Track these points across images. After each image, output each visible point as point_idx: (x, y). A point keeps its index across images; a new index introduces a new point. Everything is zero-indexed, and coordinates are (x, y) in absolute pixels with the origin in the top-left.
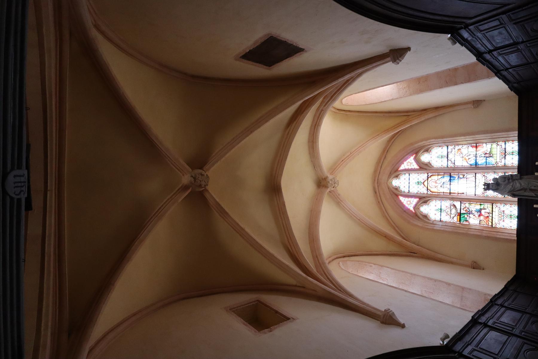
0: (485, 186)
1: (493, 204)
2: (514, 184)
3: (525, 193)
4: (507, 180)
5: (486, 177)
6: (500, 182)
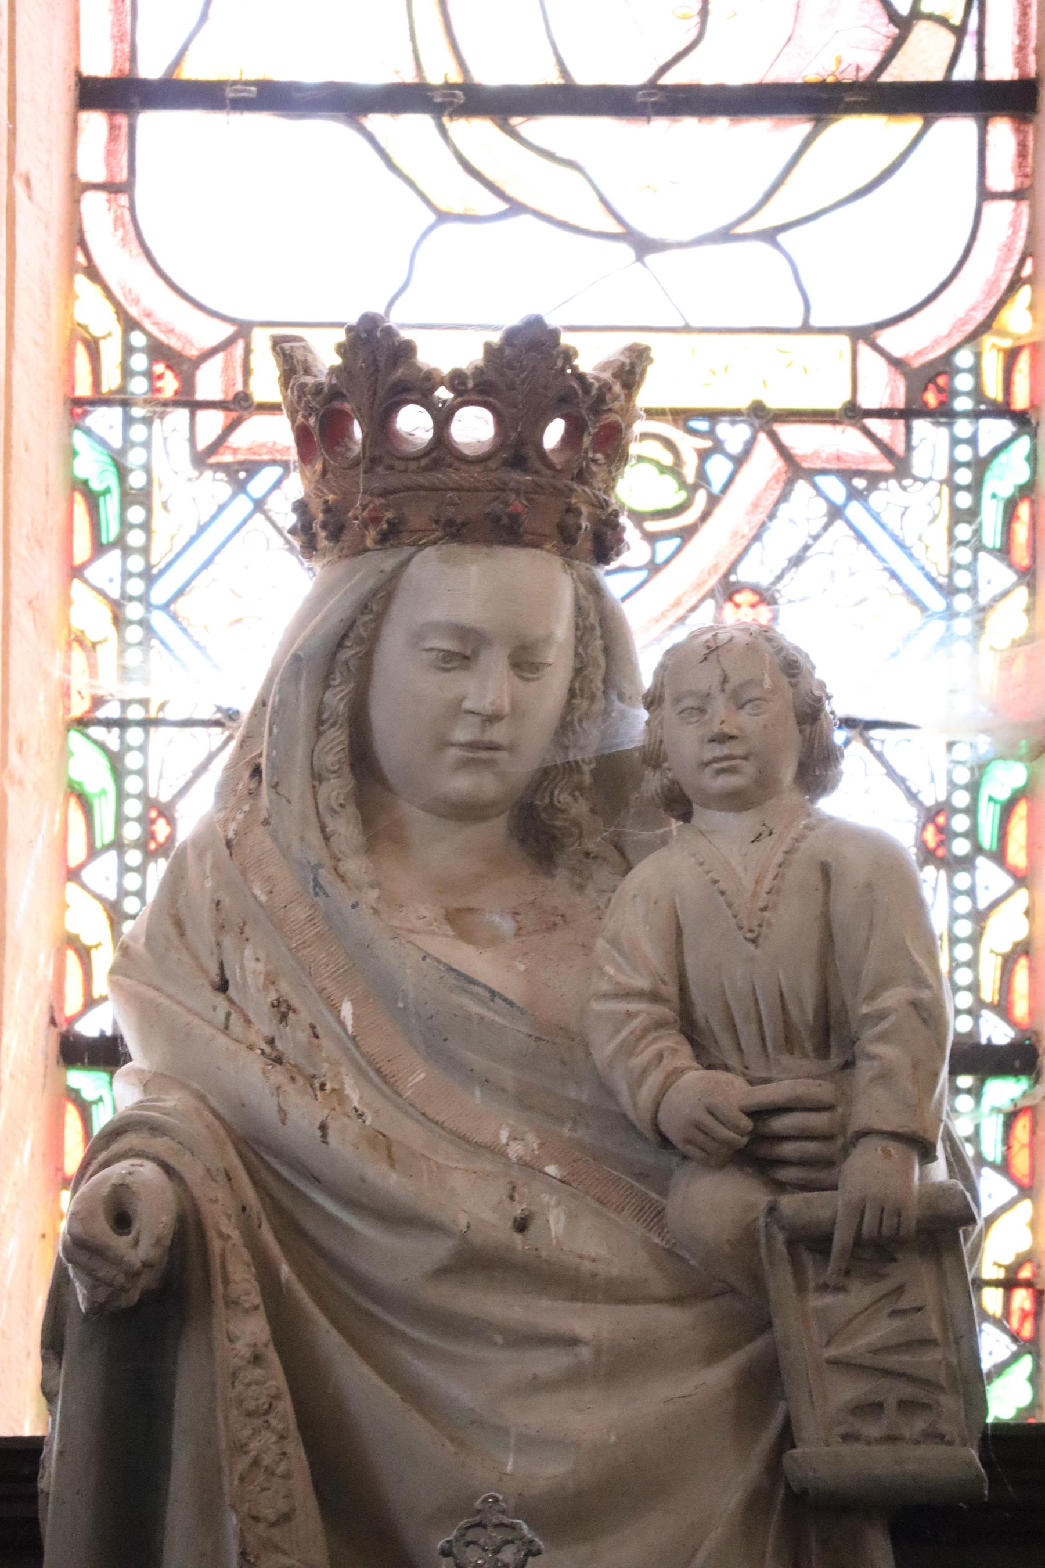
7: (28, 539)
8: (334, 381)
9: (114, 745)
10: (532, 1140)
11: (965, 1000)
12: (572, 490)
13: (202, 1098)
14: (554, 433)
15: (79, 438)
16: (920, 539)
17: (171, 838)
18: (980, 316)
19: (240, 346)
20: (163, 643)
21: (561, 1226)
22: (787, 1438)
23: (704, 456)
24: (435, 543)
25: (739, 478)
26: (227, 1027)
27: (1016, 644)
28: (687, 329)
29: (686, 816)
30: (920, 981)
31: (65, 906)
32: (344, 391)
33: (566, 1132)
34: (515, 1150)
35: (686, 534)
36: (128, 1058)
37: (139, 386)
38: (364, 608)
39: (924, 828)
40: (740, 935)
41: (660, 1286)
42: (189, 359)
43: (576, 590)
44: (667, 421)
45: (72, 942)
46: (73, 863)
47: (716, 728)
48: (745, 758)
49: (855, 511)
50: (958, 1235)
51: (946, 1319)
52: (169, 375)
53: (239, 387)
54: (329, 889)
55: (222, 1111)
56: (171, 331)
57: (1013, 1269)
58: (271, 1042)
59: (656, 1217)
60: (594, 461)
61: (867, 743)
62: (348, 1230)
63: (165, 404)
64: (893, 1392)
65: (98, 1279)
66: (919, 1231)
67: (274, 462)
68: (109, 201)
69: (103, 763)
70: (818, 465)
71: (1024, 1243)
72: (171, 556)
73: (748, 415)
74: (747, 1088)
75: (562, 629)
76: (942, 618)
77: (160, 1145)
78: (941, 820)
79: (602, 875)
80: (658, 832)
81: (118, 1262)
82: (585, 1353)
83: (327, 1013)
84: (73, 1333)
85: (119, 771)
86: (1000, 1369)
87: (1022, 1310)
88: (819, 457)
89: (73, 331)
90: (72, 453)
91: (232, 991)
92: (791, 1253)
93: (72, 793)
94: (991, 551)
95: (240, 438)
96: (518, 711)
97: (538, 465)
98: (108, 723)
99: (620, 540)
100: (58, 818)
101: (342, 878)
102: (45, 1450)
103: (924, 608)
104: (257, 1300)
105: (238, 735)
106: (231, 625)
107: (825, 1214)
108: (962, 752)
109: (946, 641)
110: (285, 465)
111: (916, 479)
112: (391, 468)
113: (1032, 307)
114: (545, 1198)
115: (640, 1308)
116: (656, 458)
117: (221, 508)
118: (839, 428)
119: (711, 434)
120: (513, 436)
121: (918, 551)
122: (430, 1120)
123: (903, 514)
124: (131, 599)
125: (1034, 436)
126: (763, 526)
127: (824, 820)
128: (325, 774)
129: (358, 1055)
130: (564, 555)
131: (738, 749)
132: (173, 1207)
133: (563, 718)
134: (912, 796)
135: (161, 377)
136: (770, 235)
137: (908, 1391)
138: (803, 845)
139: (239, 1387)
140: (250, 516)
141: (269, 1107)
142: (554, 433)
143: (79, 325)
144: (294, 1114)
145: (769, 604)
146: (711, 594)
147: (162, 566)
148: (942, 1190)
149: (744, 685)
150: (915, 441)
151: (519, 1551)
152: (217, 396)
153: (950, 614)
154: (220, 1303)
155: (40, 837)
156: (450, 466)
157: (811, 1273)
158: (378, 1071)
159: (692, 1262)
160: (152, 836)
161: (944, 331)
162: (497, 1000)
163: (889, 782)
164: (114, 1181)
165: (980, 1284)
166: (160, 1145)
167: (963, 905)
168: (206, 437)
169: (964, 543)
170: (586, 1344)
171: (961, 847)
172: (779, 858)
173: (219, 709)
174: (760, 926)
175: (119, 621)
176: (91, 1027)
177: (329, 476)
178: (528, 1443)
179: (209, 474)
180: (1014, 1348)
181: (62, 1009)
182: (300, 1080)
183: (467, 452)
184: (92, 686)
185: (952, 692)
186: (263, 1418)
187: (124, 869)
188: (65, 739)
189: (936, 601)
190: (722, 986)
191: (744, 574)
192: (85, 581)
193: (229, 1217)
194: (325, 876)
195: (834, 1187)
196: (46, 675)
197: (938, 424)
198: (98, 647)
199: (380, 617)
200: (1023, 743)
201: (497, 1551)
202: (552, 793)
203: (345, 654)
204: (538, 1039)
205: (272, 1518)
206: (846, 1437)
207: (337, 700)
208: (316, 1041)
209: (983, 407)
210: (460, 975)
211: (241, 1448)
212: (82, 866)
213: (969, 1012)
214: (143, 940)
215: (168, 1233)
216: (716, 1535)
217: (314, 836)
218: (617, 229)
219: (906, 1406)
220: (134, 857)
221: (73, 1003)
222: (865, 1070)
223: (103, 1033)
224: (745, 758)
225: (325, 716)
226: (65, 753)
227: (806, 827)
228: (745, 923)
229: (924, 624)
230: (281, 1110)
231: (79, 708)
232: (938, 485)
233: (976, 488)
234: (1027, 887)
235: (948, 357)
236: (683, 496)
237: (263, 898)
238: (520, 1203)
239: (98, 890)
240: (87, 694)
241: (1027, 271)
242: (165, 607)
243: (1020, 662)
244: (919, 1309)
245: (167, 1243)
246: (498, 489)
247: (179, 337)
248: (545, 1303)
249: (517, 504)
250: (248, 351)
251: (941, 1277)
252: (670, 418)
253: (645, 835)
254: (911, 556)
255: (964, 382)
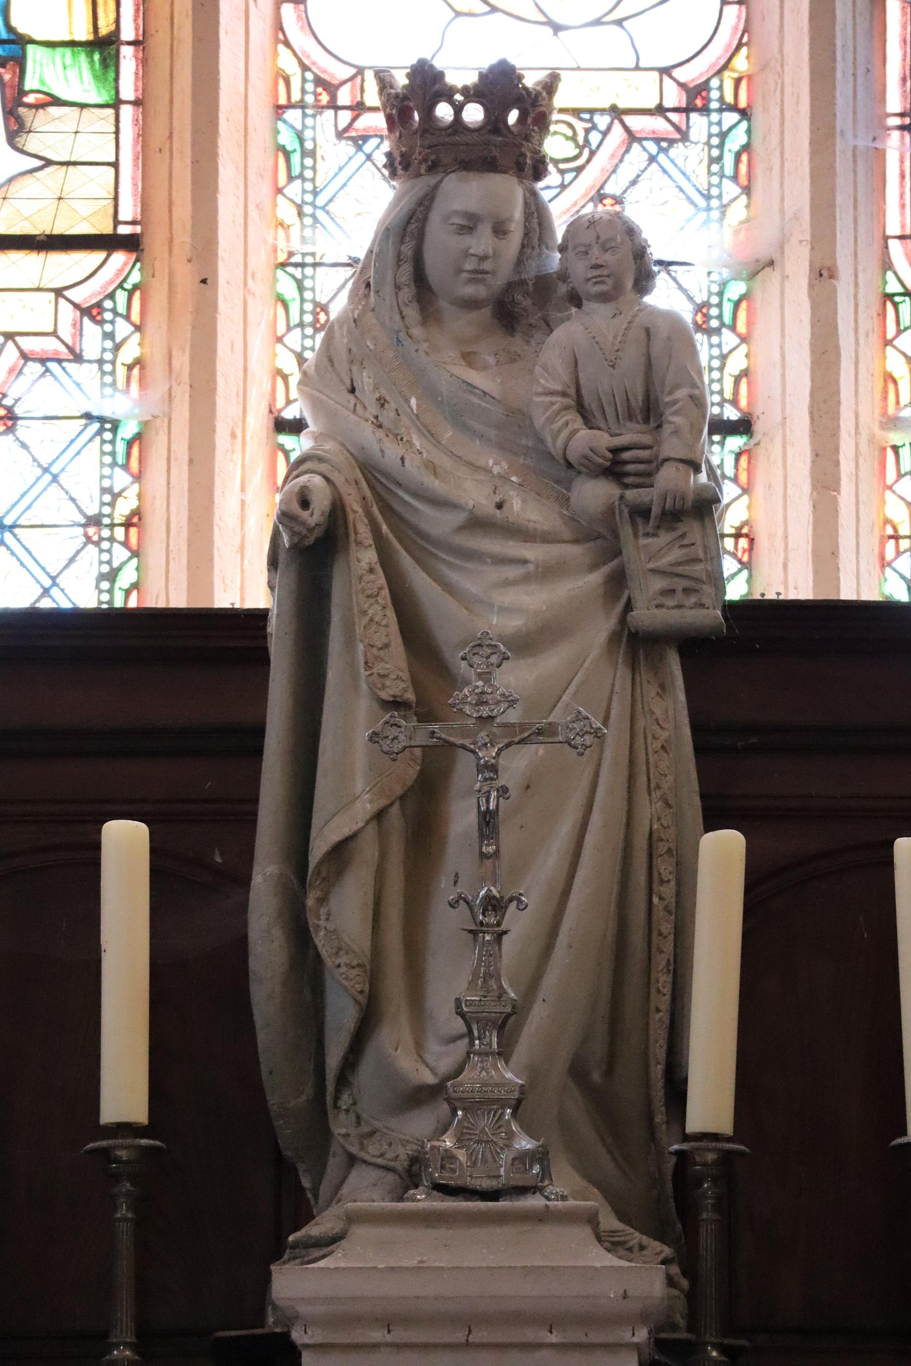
0: (473, 94)
1: (131, 244)
2: (532, 552)
3: (364, 706)
4: (603, 440)
5: (658, 124)
6: (559, 333)
7: (256, 174)
8: (405, 92)
9: (299, 276)
10: (505, 465)
11: (716, 398)
12: (522, 145)
13: (343, 445)
14: (513, 117)
15: (280, 125)
16: (694, 172)
17: (327, 321)
18: (722, 62)
19: (359, 79)
20: (322, 225)
21: (519, 506)
22: (629, 607)
23: (587, 131)
24: (454, 171)
25: (605, 142)
26: (355, 410)
27: (741, 223)
28: (578, 69)
29: (579, 306)
30: (694, 386)
31: (275, 355)
32: (410, 96)
33: (521, 461)
34: (496, 470)
35: (579, 170)
36: (307, 426)
37: (309, 99)
38: (420, 203)
39: (696, 314)
40: (606, 363)
41: (567, 534)
42: (334, 85)
43: (524, 194)
44: (570, 114)
45: (279, 373)
46: (279, 334)
47: (594, 262)
48: (608, 276)
49: (662, 158)
50: (712, 508)
51: (706, 549)
52: (324, 93)
53: (359, 99)
54: (405, 343)
55: (353, 451)
56: (325, 72)
57: (740, 528)
58: (376, 417)
59: (565, 501)
60: (533, 130)
61: (668, 273)
62: (416, 510)
63: (323, 107)
64: (681, 583)
65: (294, 532)
66: (693, 507)
67: (376, 136)
68: (295, 8)
69: (294, 285)
70: (644, 135)
71: (744, 516)
72: (326, 182)
73: (609, 111)
74: (610, 438)
75: (518, 214)
76: (704, 210)
77: (323, 467)
78: (704, 310)
79: (538, 336)
80: (565, 314)
81: (303, 523)
82: (531, 567)
83: (403, 403)
84: (282, 557)
85: (301, 288)
86: (733, 576)
87: (743, 548)
88: (644, 132)
89: (277, 72)
90: (277, 132)
91: (357, 393)
92: (630, 517)
93: (279, 300)
94: (728, 178)
95: (359, 124)
96: (496, 254)
97: (505, 132)
98: (296, 265)
99: (546, 170)
100: (272, 312)
101: (411, 337)
102: (270, 614)
103: (696, 206)
104: (371, 542)
105: (358, 271)
106: (355, 216)
107: (647, 499)
108: (715, 277)
109: (707, 221)
110: (381, 137)
111: (692, 142)
112: (433, 134)
113: (748, 57)
114: (511, 493)
115: (558, 545)
116: (564, 132)
117: (350, 159)
118: (654, 117)
119: (591, 120)
120: (493, 118)
121: (693, 178)
122: (455, 455)
123: (686, 159)
124: (307, 203)
125: (749, 120)
126: (617, 166)
127: (647, 307)
128: (402, 286)
129: (419, 425)
130: (518, 177)
131: (605, 272)
132: (330, 497)
133: (518, 259)
134: (690, 299)
135: (320, 94)
136: (619, 23)
137: (686, 583)
138: (637, 319)
139: (363, 584)
140: (364, 163)
141: (376, 447)
142: (513, 117)
143: (280, 69)
144: (388, 452)
145: (620, 204)
146: (592, 199)
147: (322, 187)
148: (705, 487)
149: (607, 240)
150: (691, 124)
151: (499, 657)
152: (348, 103)
153: (709, 209)
154: (353, 545)
155: (263, 321)
156: (462, 133)
157: (640, 528)
158: (429, 431)
159: (583, 523)
160: (318, 321)
161: (705, 69)
162: (487, 396)
163: (679, 292)
164: (300, 484)
165: (723, 536)
166: (323, 467)
167: (716, 352)
168: (342, 125)
169: (715, 174)
170: (531, 562)
171: (714, 323)
172: (625, 325)
173: (350, 258)
174: (616, 359)
175: (301, 214)
176: (290, 413)
177: (403, 138)
178: (504, 610)
179: (344, 142)
180: (739, 566)
181: (275, 405)
182: (391, 436)
183: (470, 126)
184: (288, 247)
185: (710, 247)
186: (375, 599)
187: (304, 337)
188: (275, 273)
189: (702, 203)
190: (597, 388)
191: (608, 189)
192: (284, 196)
193: (357, 502)
194: (402, 335)
195: (652, 486)
196: (265, 241)
197: (702, 115)
198: (291, 228)
199: (428, 209)
200: (744, 272)
201: (488, 657)
202: (513, 295)
203: (412, 227)
204: (508, 415)
205: (380, 646)
206: (657, 606)
207: (407, 249)
208: (398, 417)
209: (724, 107)
210: (469, 384)
211: (364, 613)
212: (284, 335)
213: (718, 404)
214: (313, 368)
215: (327, 510)
216: (594, 653)
217: (397, 317)
218: (544, 19)
219: (687, 591)
220: (309, 331)
221: (280, 402)
222: (667, 429)
223: (295, 417)
224: (608, 276)
225: (402, 257)
226: (275, 280)
227: (638, 310)
228: (609, 358)
229: (696, 213)
230: (382, 451)
231: (282, 258)
232: (702, 146)
233: (721, 146)
234: (747, 343)
235: (708, 81)
236: (577, 151)
237: (372, 347)
238: (499, 495)
239: (292, 347)
240: (285, 251)
241: (745, 39)
242: (323, 208)
243: (743, 232)
244: (693, 544)
245: (327, 514)
246: (486, 144)
247: (329, 74)
248: (511, 543)
249: (495, 152)
250: (363, 80)
251: (704, 527)
252: (571, 112)
253: (559, 315)
254: (689, 180)
255: (714, 95)
